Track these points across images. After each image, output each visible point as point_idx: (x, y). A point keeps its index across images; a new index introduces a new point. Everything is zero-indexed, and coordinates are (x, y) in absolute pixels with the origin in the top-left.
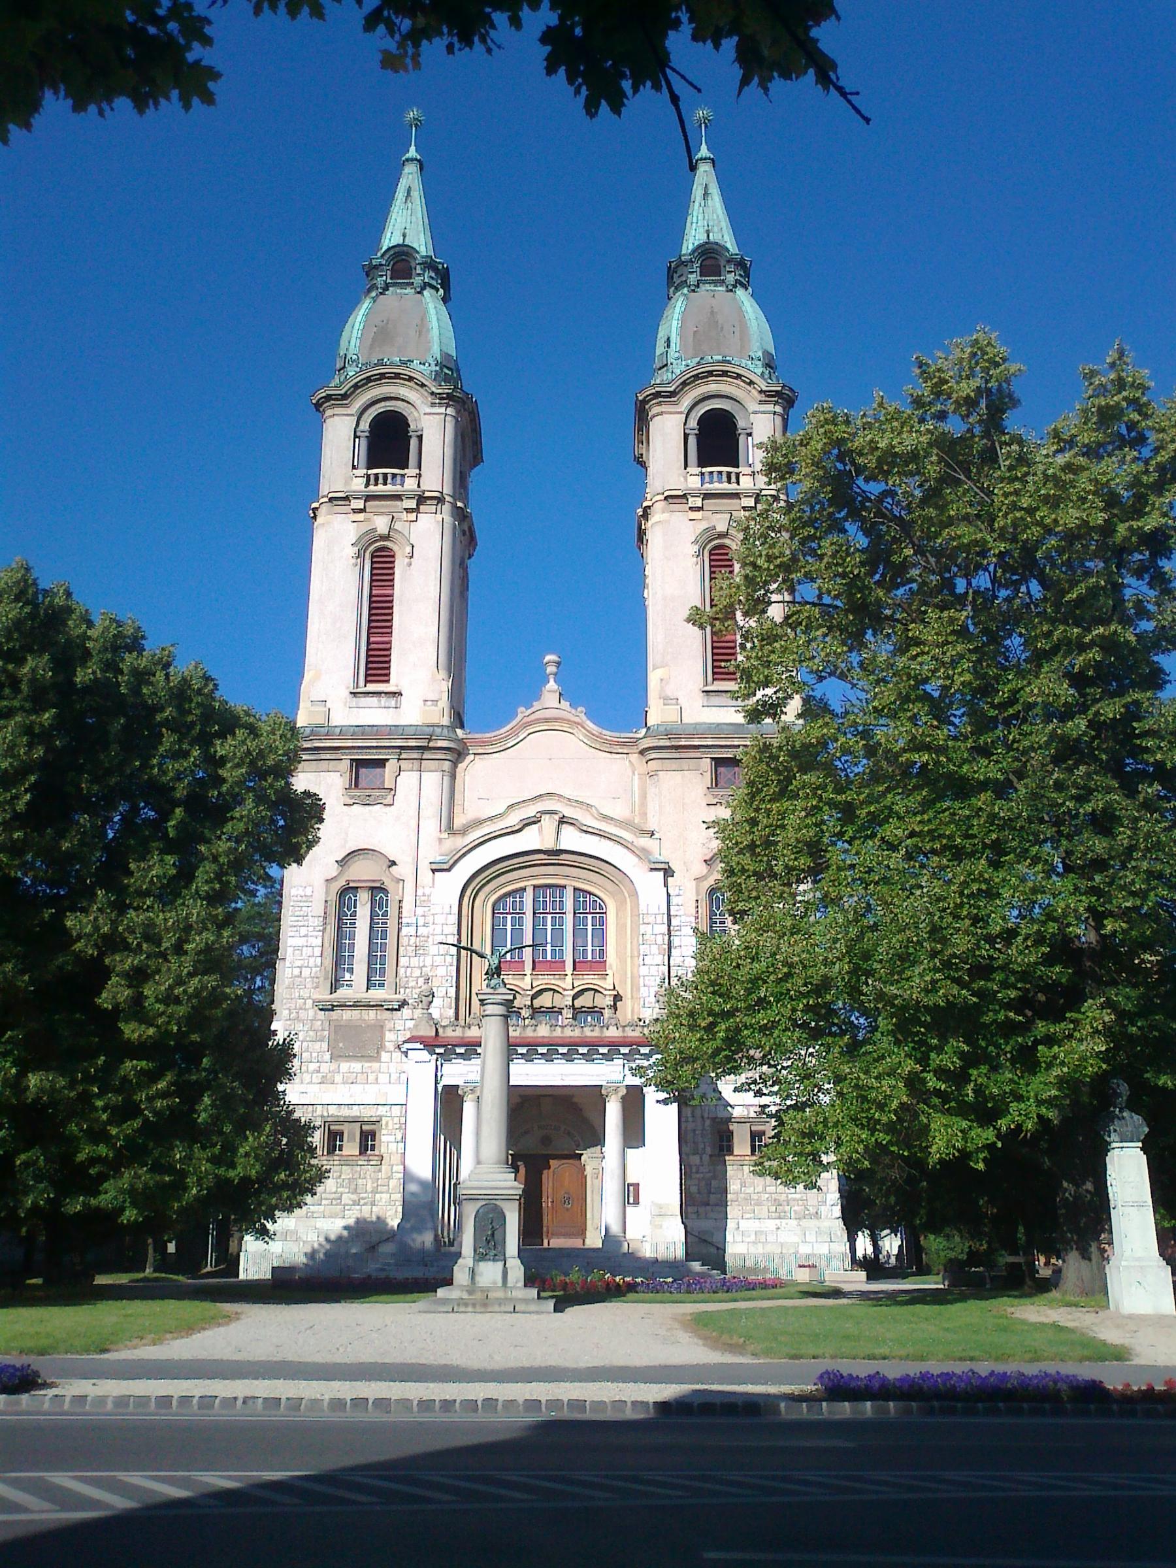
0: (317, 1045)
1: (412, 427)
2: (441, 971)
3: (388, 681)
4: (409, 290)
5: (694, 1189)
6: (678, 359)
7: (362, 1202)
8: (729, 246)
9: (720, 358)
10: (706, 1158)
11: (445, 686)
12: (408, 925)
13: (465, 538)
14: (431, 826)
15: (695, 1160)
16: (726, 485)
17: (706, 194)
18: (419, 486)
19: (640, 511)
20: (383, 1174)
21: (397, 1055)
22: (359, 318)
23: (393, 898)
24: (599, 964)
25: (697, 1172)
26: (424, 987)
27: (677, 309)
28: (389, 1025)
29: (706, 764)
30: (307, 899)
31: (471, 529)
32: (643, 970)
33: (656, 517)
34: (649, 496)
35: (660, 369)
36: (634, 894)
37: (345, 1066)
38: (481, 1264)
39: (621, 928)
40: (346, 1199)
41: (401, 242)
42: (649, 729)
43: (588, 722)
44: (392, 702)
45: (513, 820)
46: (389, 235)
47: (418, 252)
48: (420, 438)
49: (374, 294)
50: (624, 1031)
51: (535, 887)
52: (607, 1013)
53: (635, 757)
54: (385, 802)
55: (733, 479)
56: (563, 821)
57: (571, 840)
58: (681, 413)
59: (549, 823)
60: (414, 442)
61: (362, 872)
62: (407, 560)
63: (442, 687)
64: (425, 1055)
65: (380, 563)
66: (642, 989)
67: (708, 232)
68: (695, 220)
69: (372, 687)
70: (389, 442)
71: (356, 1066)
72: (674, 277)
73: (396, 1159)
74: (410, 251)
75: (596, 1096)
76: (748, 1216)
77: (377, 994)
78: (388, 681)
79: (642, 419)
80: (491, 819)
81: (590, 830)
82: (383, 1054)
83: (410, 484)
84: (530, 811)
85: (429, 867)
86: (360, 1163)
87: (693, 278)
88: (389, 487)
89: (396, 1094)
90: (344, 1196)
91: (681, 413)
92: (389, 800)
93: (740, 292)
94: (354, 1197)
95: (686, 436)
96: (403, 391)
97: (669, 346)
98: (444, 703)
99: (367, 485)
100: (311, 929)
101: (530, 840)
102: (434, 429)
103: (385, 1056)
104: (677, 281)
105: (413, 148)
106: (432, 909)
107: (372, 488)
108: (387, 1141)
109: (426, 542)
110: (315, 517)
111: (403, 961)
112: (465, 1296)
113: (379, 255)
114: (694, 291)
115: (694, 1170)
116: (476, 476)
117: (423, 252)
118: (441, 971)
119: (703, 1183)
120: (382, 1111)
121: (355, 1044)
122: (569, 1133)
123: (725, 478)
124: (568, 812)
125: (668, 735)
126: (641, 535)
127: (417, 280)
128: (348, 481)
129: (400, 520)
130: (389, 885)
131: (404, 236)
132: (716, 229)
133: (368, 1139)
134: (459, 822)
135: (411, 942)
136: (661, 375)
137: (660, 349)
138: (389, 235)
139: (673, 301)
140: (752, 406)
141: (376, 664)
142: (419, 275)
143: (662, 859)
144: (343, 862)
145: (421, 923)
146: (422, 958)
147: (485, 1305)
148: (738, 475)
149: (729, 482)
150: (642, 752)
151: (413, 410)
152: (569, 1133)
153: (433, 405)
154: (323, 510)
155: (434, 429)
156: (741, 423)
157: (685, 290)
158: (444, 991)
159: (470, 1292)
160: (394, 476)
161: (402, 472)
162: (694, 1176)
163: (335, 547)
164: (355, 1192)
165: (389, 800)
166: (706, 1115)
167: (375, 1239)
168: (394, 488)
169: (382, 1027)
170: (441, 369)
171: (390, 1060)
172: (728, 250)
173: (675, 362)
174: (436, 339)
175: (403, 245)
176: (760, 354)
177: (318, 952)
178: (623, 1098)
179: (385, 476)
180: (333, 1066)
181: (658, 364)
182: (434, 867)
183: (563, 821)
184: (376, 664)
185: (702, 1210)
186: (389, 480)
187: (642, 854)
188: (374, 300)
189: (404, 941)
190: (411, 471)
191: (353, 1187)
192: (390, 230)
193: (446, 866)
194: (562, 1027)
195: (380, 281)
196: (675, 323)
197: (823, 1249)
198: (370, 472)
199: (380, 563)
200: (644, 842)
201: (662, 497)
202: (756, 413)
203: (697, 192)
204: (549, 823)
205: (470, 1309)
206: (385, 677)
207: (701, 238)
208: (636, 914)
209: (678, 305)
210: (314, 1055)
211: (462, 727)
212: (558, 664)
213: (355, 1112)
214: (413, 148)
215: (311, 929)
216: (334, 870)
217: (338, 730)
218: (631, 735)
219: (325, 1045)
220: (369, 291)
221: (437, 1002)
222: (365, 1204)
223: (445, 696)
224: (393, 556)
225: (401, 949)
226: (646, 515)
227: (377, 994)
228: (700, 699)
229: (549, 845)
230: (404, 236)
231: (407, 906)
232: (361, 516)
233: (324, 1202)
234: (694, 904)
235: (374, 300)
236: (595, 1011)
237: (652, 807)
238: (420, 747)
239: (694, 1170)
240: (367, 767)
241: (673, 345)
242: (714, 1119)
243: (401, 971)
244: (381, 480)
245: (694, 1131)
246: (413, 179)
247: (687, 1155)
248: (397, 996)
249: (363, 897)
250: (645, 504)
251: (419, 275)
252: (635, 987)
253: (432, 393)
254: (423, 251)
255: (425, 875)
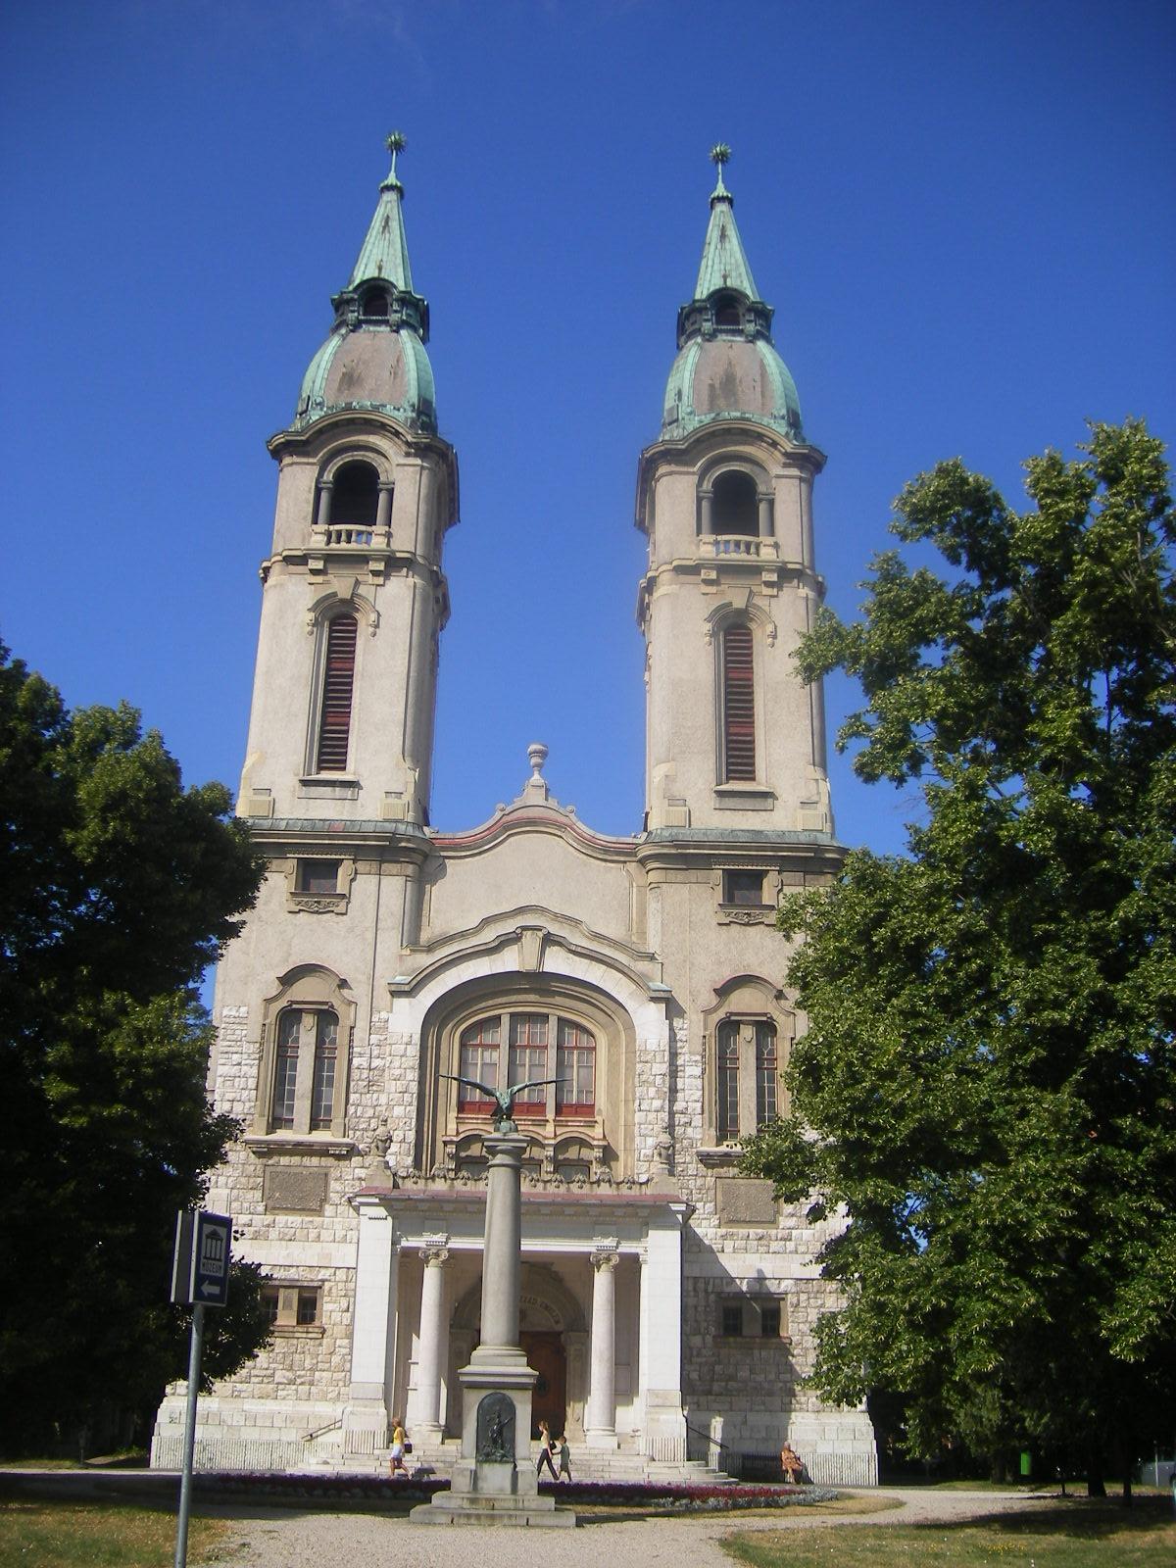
0: (250, 1195)
1: (383, 478)
2: (398, 1111)
3: (344, 769)
4: (384, 328)
5: (694, 1376)
6: (690, 413)
7: (299, 1381)
8: (749, 292)
9: (738, 414)
10: (709, 1339)
11: (412, 776)
12: (361, 1055)
13: (437, 606)
14: (391, 941)
15: (696, 1341)
16: (743, 556)
17: (723, 236)
18: (388, 544)
19: (643, 582)
20: (323, 1349)
21: (344, 1209)
22: (326, 357)
23: (344, 1022)
24: (586, 1109)
25: (698, 1355)
26: (381, 1129)
27: (690, 360)
28: (334, 1173)
29: (717, 875)
30: (241, 1021)
31: (445, 596)
32: (638, 1117)
33: (661, 591)
34: (654, 566)
35: (670, 424)
36: (630, 1027)
37: (281, 1219)
38: (486, 1466)
39: (613, 1066)
40: (279, 1376)
41: (376, 275)
42: (650, 833)
43: (579, 824)
44: (349, 793)
45: (489, 935)
46: (362, 268)
47: (395, 287)
48: (391, 492)
49: (343, 331)
50: (618, 1188)
51: (512, 1015)
52: (595, 1168)
53: (632, 867)
54: (336, 910)
55: (753, 550)
56: (549, 940)
57: (557, 962)
58: (693, 473)
59: (531, 942)
60: (382, 497)
61: (306, 991)
62: (371, 629)
63: (406, 779)
64: (382, 1212)
65: (338, 623)
66: (638, 1140)
67: (725, 277)
68: (710, 263)
69: (325, 775)
70: (354, 495)
71: (295, 1220)
72: (686, 323)
73: (339, 1331)
74: (387, 285)
75: (586, 1265)
76: (757, 1408)
77: (321, 1136)
78: (344, 769)
79: (647, 473)
80: (463, 935)
81: (579, 950)
82: (327, 1206)
83: (378, 543)
84: (509, 926)
85: (387, 988)
86: (297, 1335)
87: (707, 326)
88: (353, 545)
89: (344, 1255)
90: (278, 1374)
91: (693, 473)
92: (341, 908)
93: (761, 344)
94: (290, 1375)
95: (699, 500)
96: (374, 440)
97: (680, 399)
98: (408, 797)
99: (328, 542)
100: (245, 1056)
101: (509, 961)
102: (405, 481)
103: (329, 1209)
104: (690, 329)
105: (392, 174)
106: (391, 1033)
107: (333, 545)
108: (329, 1309)
109: (392, 607)
110: (265, 579)
111: (353, 1097)
112: (466, 1504)
113: (351, 288)
114: (709, 340)
115: (695, 1353)
116: (452, 536)
117: (401, 286)
118: (398, 1111)
119: (705, 1369)
120: (324, 1274)
121: (299, 1197)
122: (547, 1307)
123: (742, 547)
124: (554, 928)
125: (675, 843)
126: (643, 612)
127: (394, 317)
128: (305, 538)
129: (365, 583)
130: (340, 1009)
131: (380, 268)
132: (734, 274)
133: (307, 1309)
134: (425, 936)
135: (364, 1076)
136: (671, 431)
137: (669, 402)
138: (362, 268)
139: (684, 350)
140: (776, 469)
141: (330, 745)
142: (396, 311)
143: (664, 987)
144: (288, 980)
145: (375, 1053)
146: (375, 1096)
147: (492, 1517)
148: (757, 546)
149: (748, 553)
150: (642, 862)
151: (383, 459)
152: (547, 1307)
153: (408, 455)
154: (276, 570)
155: (405, 481)
156: (761, 488)
157: (699, 340)
158: (404, 1133)
159: (473, 1501)
160: (359, 533)
161: (369, 529)
162: (694, 1360)
163: (287, 609)
164: (291, 1369)
165: (341, 908)
166: (710, 1289)
167: (313, 1426)
168: (359, 547)
169: (326, 1175)
170: (418, 415)
171: (336, 1217)
172: (747, 297)
173: (687, 417)
174: (414, 383)
175: (378, 279)
176: (784, 412)
177: (252, 1083)
178: (616, 1268)
179: (349, 534)
180: (269, 1218)
181: (667, 418)
182: (393, 988)
183: (549, 940)
184: (330, 745)
185: (703, 1399)
186: (353, 538)
187: (639, 981)
188: (344, 337)
189: (355, 1074)
190: (379, 528)
191: (288, 1362)
192: (364, 261)
193: (407, 988)
194: (546, 1182)
195: (351, 317)
196: (687, 374)
197: (846, 1449)
198: (332, 528)
199: (338, 623)
200: (642, 966)
201: (670, 567)
202: (778, 477)
203: (713, 233)
204: (531, 942)
205: (473, 1521)
206: (341, 765)
207: (717, 283)
208: (631, 1050)
209: (692, 353)
210: (246, 1205)
211: (428, 825)
212: (543, 754)
213: (292, 1274)
214: (392, 174)
215: (245, 1056)
216: (274, 988)
217: (284, 823)
218: (630, 840)
219: (258, 1194)
220: (338, 327)
221: (394, 1147)
222: (302, 1384)
223: (411, 788)
224: (355, 625)
225: (352, 1084)
226: (650, 587)
227: (321, 1136)
228: (713, 801)
229: (530, 965)
230: (380, 268)
231: (359, 1034)
232: (319, 579)
233: (253, 1379)
234: (701, 1040)
235: (344, 337)
236: (584, 1166)
237: (653, 925)
238: (382, 849)
239: (695, 1353)
240: (318, 871)
241: (685, 398)
242: (719, 1294)
243: (351, 1110)
244: (344, 537)
245: (696, 1307)
246: (392, 209)
247: (687, 1335)
248: (346, 1140)
249: (747, 1032)
250: (649, 574)
251: (396, 311)
252: (629, 1137)
253: (407, 443)
254: (401, 286)
255: (382, 993)
